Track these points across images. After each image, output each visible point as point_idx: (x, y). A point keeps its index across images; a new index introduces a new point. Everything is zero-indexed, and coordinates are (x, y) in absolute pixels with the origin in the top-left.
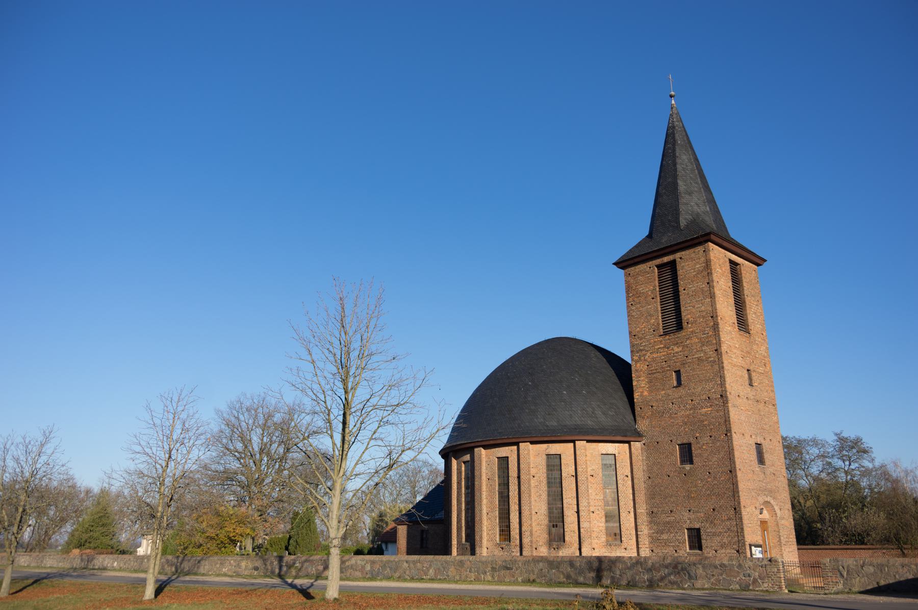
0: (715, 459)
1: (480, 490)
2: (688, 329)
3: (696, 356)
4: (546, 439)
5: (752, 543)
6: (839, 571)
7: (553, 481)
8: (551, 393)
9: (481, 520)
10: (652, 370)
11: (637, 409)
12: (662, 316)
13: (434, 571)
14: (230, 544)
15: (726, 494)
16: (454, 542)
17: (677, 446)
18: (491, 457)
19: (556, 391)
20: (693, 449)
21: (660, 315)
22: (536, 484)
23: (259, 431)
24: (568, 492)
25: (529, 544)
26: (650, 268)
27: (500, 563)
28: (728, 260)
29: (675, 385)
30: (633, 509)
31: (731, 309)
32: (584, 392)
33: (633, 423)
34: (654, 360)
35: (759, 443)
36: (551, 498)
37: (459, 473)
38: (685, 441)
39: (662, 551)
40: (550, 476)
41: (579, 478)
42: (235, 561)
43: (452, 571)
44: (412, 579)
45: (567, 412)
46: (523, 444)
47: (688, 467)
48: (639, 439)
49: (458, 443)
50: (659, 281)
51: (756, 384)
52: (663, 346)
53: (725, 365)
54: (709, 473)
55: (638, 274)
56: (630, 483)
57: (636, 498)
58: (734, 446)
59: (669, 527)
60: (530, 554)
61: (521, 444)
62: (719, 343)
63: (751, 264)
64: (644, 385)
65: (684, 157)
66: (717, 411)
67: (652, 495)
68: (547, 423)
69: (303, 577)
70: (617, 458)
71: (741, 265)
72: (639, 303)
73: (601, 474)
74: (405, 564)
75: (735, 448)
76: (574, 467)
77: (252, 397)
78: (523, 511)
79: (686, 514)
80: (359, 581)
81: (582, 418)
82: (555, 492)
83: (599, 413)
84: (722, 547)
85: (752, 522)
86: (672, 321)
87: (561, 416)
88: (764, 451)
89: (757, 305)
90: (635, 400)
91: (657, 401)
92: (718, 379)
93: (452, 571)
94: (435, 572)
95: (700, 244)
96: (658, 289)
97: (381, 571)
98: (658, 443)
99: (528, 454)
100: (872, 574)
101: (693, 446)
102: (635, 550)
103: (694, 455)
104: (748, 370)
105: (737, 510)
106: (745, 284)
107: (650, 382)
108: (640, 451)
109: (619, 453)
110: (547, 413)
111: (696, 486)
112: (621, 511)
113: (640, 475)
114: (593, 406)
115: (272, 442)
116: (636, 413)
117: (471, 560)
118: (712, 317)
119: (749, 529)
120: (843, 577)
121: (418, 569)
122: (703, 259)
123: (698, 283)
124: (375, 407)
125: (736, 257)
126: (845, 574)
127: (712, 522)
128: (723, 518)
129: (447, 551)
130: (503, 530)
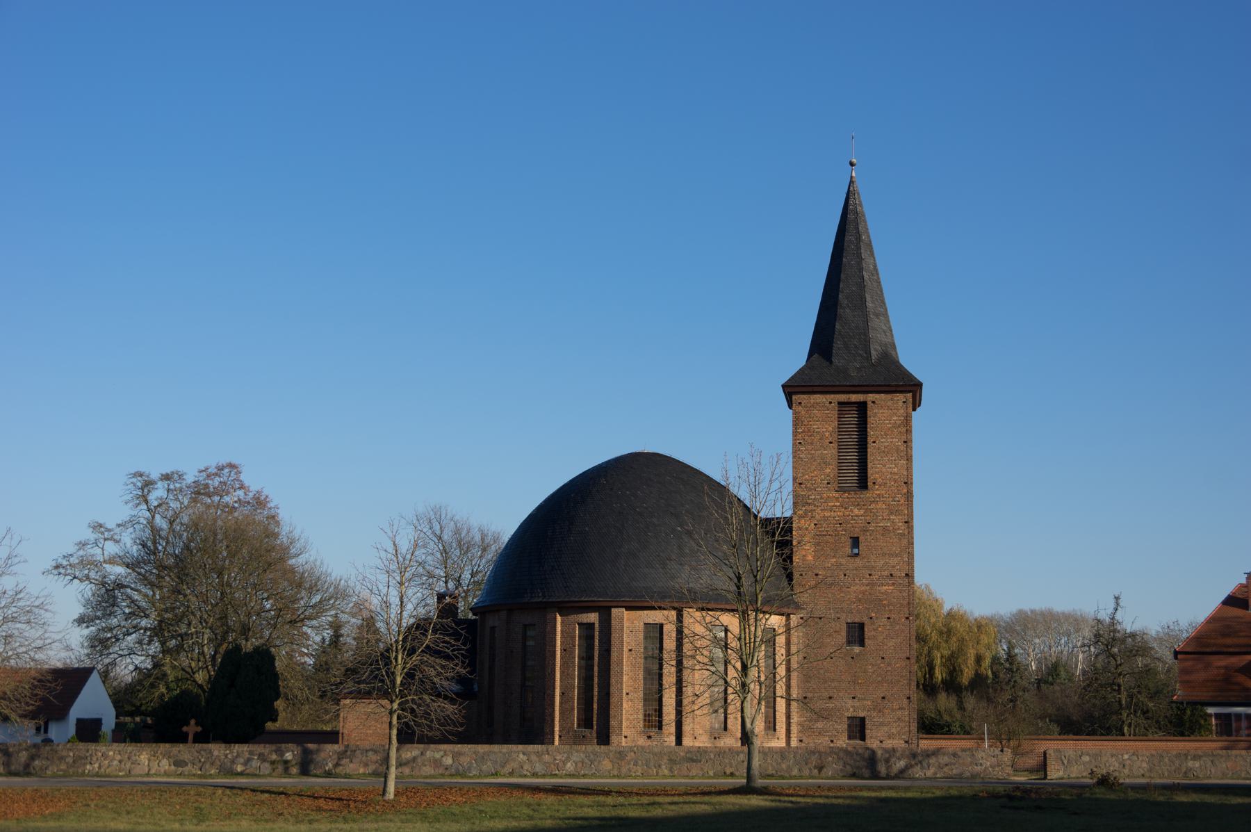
0: (891, 644)
2: (874, 491)
6: (1062, 760)
10: (820, 531)
13: (574, 765)
15: (900, 681)
20: (866, 629)
34: (825, 519)
38: (857, 620)
39: (810, 743)
47: (857, 649)
52: (838, 504)
55: (812, 406)
69: (275, 777)
72: (812, 444)
74: (521, 756)
79: (850, 702)
84: (889, 737)
86: (852, 476)
103: (866, 637)
123: (892, 438)
126: (1066, 762)
130: (649, 714)
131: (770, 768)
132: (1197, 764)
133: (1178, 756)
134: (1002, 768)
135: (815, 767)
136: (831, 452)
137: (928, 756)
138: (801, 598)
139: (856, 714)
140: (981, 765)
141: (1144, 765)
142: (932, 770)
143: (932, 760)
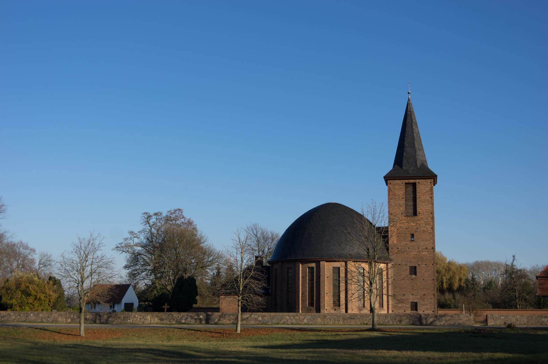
3: (422, 229)
6: (493, 318)
18: (329, 266)
20: (417, 269)
34: (401, 227)
47: (414, 276)
52: (406, 221)
55: (395, 184)
59: (400, 301)
72: (395, 199)
74: (287, 317)
79: (411, 296)
86: (411, 211)
91: (401, 246)
92: (432, 241)
93: (319, 320)
100: (503, 319)
101: (417, 268)
103: (417, 271)
107: (398, 237)
126: (495, 319)
128: (428, 298)
131: (381, 321)
132: (546, 320)
133: (538, 316)
135: (398, 321)
136: (403, 202)
137: (442, 317)
139: (414, 301)
143: (443, 318)
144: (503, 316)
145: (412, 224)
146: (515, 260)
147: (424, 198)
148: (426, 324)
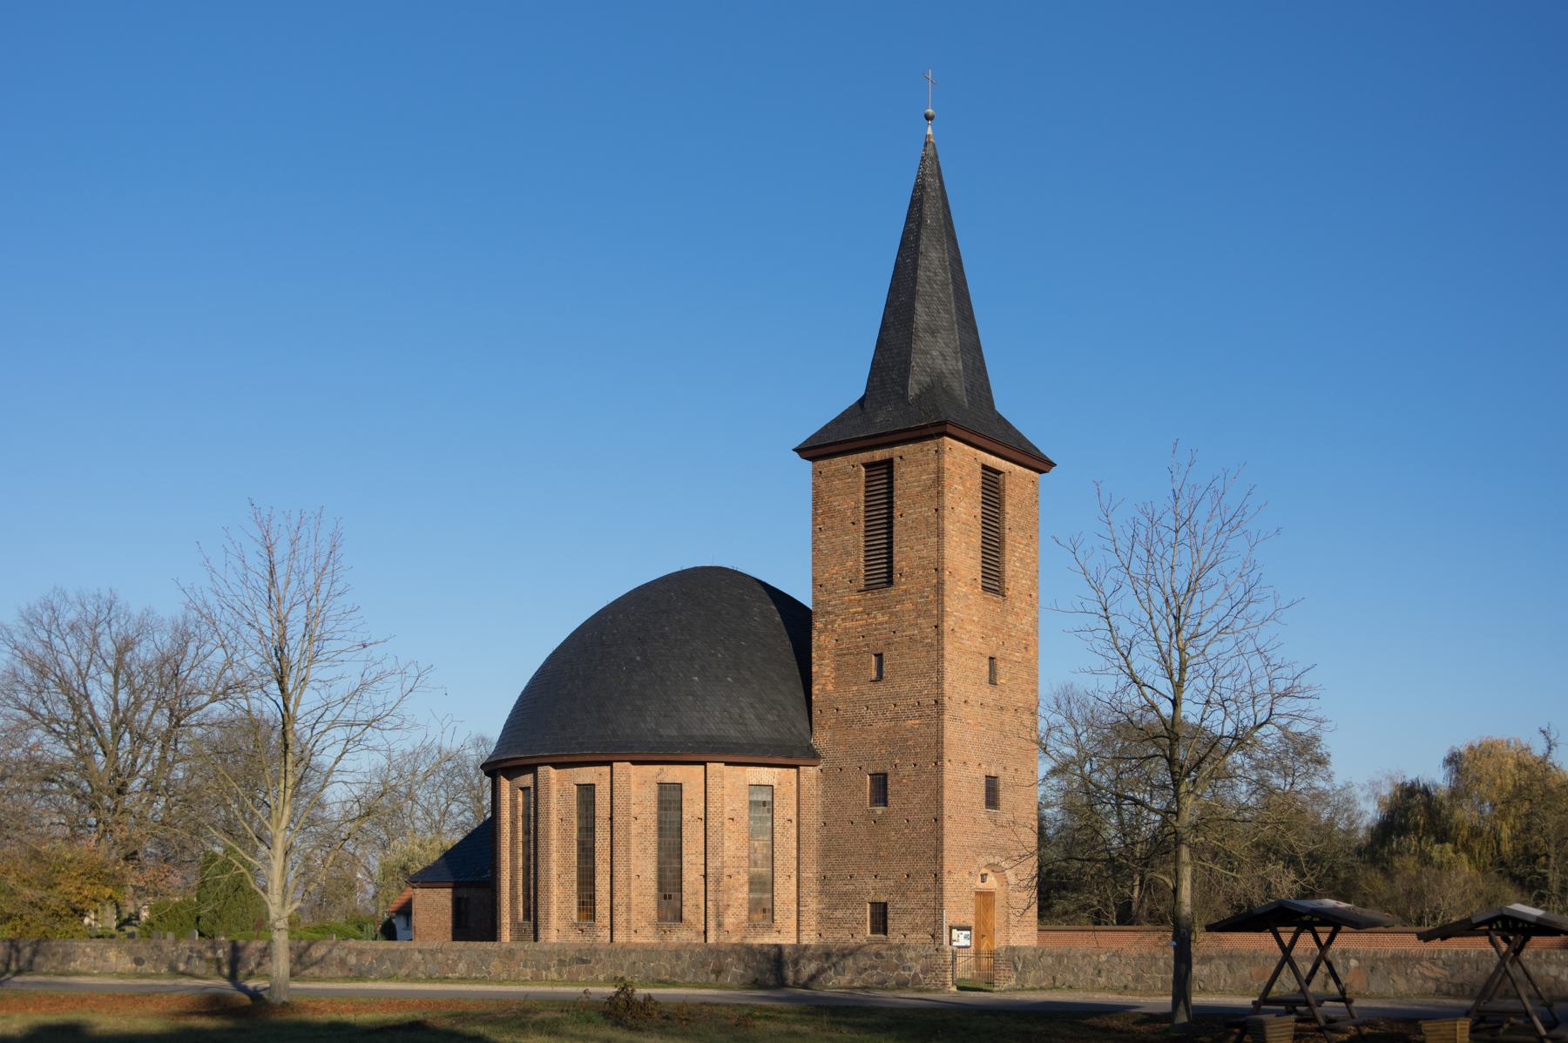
0: (916, 801)
1: (547, 837)
2: (902, 584)
3: (908, 633)
4: (656, 758)
5: (954, 924)
6: (1014, 963)
7: (668, 826)
8: (673, 679)
9: (547, 886)
10: (841, 649)
11: (816, 712)
12: (866, 556)
14: (72, 916)
16: (505, 920)
17: (868, 776)
19: (681, 675)
20: (889, 782)
21: (862, 554)
22: (640, 831)
23: (108, 678)
24: (690, 844)
25: (624, 924)
26: (853, 466)
27: (572, 953)
28: (979, 467)
29: (873, 678)
30: (795, 872)
31: (972, 556)
32: (729, 679)
33: (807, 736)
34: (846, 631)
35: (993, 775)
36: (663, 854)
37: (514, 806)
40: (663, 819)
41: (710, 823)
42: (94, 949)
43: (495, 966)
44: (430, 979)
45: (695, 713)
46: (619, 763)
47: (879, 810)
48: (814, 762)
49: (510, 757)
50: (866, 492)
51: (1002, 681)
52: (861, 609)
53: (945, 653)
54: (908, 821)
55: (833, 475)
56: (794, 831)
57: (802, 855)
58: (945, 781)
60: (624, 940)
61: (615, 764)
62: (941, 616)
63: (1027, 471)
64: (828, 674)
65: (933, 255)
66: (928, 726)
67: (825, 853)
68: (661, 730)
70: (775, 791)
71: (1007, 473)
72: (832, 528)
73: (746, 818)
74: (417, 954)
75: (946, 786)
76: (703, 804)
77: (79, 597)
78: (615, 874)
80: (337, 982)
81: (721, 725)
82: (670, 844)
83: (750, 716)
84: (913, 930)
85: (960, 894)
87: (686, 720)
88: (1001, 788)
89: (1027, 545)
90: (813, 697)
93: (495, 966)
94: (468, 967)
95: (930, 437)
96: (862, 508)
97: (375, 965)
98: (841, 769)
99: (628, 781)
101: (889, 778)
102: (795, 934)
104: (991, 658)
105: (938, 877)
106: (1008, 508)
107: (837, 669)
108: (814, 781)
109: (779, 784)
110: (662, 713)
111: (888, 840)
112: (775, 874)
113: (812, 819)
114: (742, 704)
115: (138, 705)
116: (813, 720)
117: (526, 948)
118: (936, 570)
119: (953, 905)
120: (1017, 969)
121: (439, 963)
122: (933, 466)
123: (921, 507)
124: (333, 724)
125: (999, 460)
127: (903, 894)
129: (492, 934)
131: (663, 972)
134: (936, 974)
135: (713, 971)
137: (844, 956)
138: (820, 740)
140: (910, 969)
141: (1128, 970)
142: (848, 977)
143: (850, 962)
144: (1050, 955)
145: (881, 618)
146: (1553, 747)
147: (915, 516)
148: (794, 982)
